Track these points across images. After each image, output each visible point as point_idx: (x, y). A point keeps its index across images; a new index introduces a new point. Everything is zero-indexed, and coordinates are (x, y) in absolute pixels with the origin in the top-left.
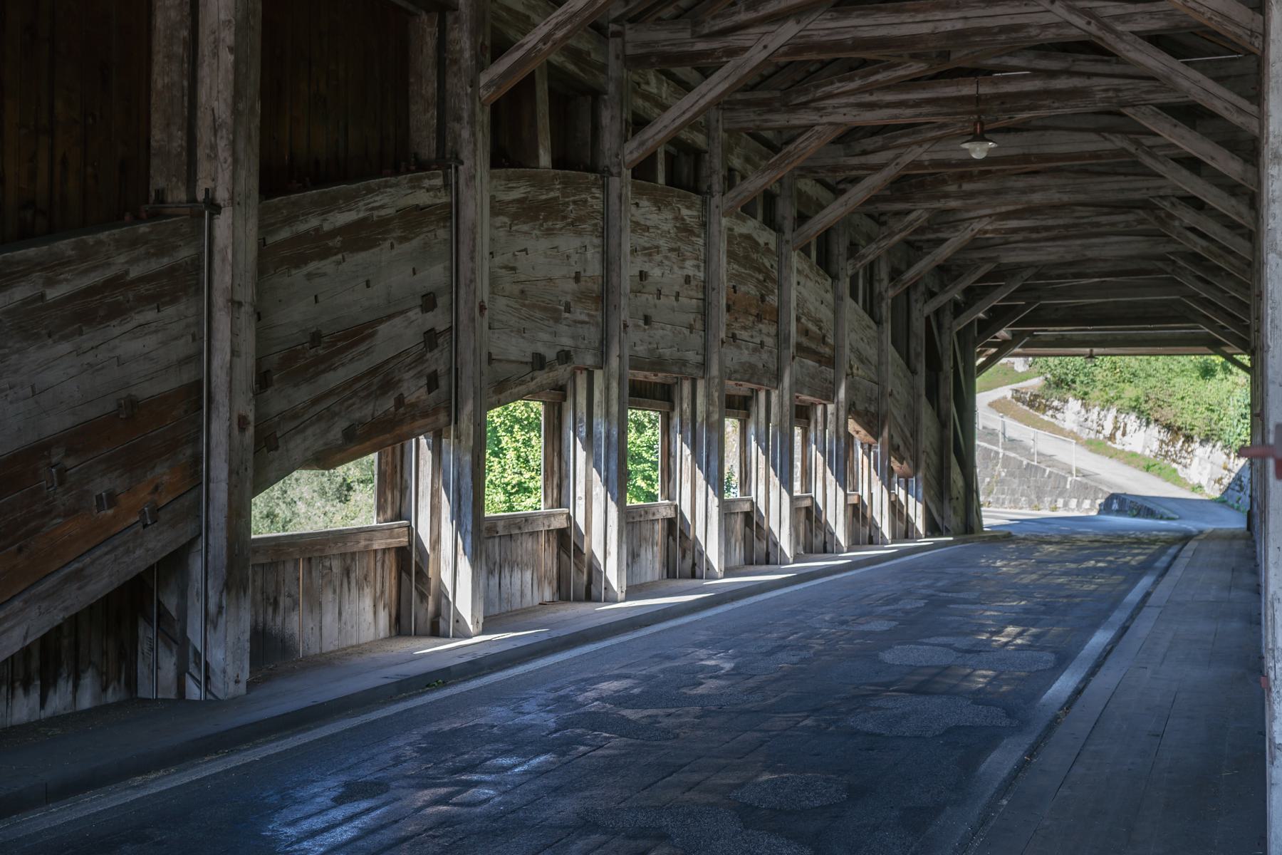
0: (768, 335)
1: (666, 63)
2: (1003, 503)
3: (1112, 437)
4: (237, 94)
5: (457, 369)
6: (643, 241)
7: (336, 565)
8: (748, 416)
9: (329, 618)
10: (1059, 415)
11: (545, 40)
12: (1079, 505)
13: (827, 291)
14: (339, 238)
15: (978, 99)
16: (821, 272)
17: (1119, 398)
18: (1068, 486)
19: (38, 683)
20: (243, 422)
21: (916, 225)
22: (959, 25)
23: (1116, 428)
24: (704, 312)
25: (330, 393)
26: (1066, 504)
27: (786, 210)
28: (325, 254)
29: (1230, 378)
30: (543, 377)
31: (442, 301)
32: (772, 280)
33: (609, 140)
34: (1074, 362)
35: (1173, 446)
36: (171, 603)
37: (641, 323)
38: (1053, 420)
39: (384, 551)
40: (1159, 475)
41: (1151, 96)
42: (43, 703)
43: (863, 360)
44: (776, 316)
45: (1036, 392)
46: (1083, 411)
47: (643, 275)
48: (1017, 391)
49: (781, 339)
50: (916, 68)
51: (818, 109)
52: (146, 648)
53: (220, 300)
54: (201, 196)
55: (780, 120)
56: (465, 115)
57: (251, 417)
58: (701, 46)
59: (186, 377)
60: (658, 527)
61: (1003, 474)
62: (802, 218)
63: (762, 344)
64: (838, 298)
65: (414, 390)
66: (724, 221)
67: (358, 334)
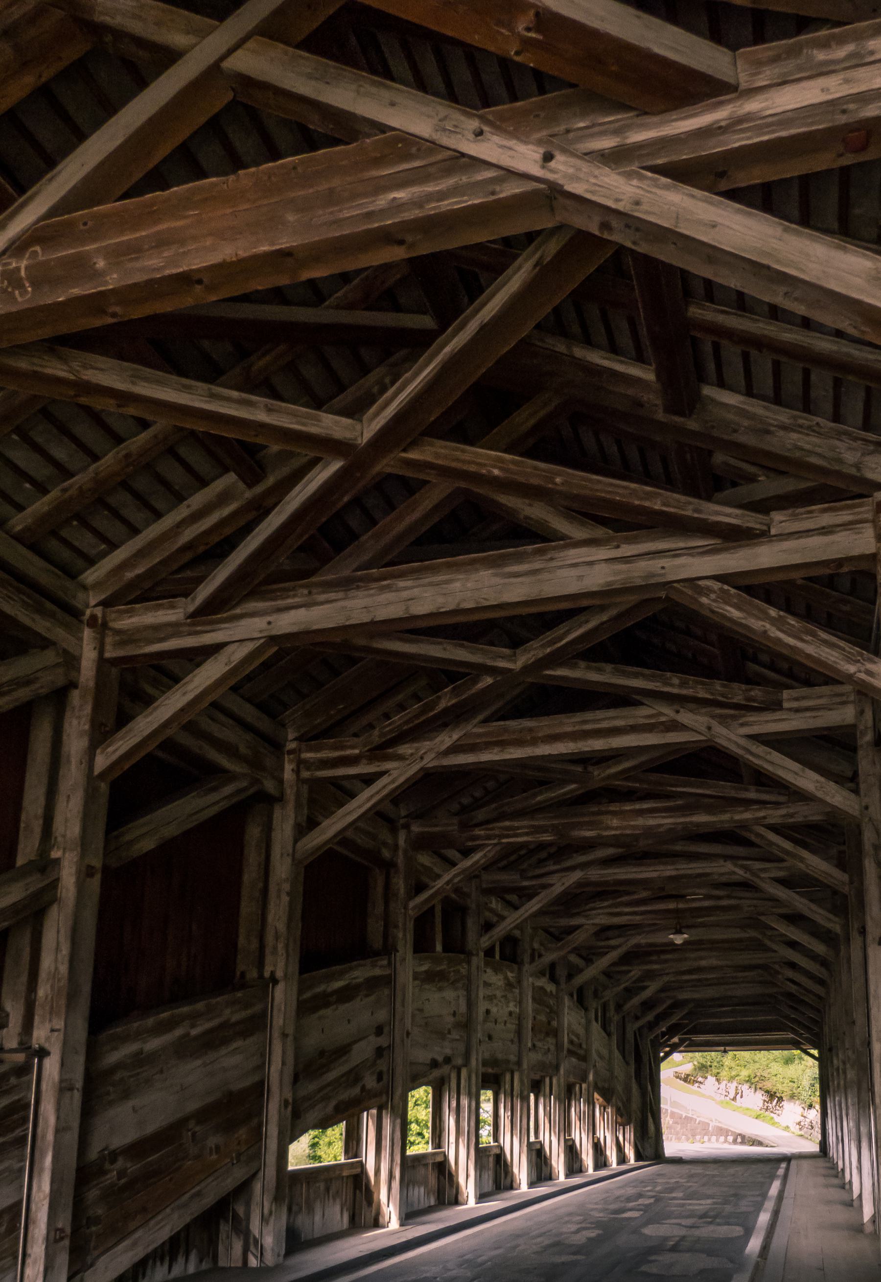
0: (552, 1044)
1: (500, 892)
2: (671, 1140)
3: (734, 1099)
4: (290, 919)
5: (393, 1069)
6: (489, 992)
7: (322, 1186)
8: (500, 1089)
9: (318, 1218)
10: (701, 1086)
11: (447, 883)
12: (717, 1140)
13: (582, 1018)
14: (334, 997)
15: (677, 911)
16: (579, 1006)
17: (738, 1075)
18: (710, 1129)
19: (168, 1258)
20: (286, 1103)
21: (634, 979)
22: (674, 873)
23: (737, 1094)
24: (519, 1032)
25: (328, 1085)
26: (709, 1140)
27: (562, 973)
28: (327, 1005)
29: (803, 1062)
30: (436, 1073)
31: (386, 1030)
32: (554, 1013)
33: (471, 935)
34: (712, 1056)
35: (771, 1103)
36: (241, 1210)
37: (487, 1039)
38: (699, 1089)
39: (347, 1177)
40: (763, 1121)
41: (774, 910)
42: (170, 1271)
43: (601, 1056)
44: (555, 1033)
45: (688, 1073)
46: (717, 1083)
47: (488, 1012)
48: (676, 1072)
49: (559, 1047)
50: (644, 894)
51: (586, 916)
52: (224, 1236)
53: (276, 1034)
54: (267, 974)
55: (564, 922)
56: (400, 925)
57: (291, 1100)
58: (526, 883)
59: (256, 1078)
60: (491, 1159)
61: (671, 1122)
62: (570, 977)
63: (549, 1049)
64: (588, 1022)
65: (370, 1082)
66: (531, 979)
67: (343, 1050)
